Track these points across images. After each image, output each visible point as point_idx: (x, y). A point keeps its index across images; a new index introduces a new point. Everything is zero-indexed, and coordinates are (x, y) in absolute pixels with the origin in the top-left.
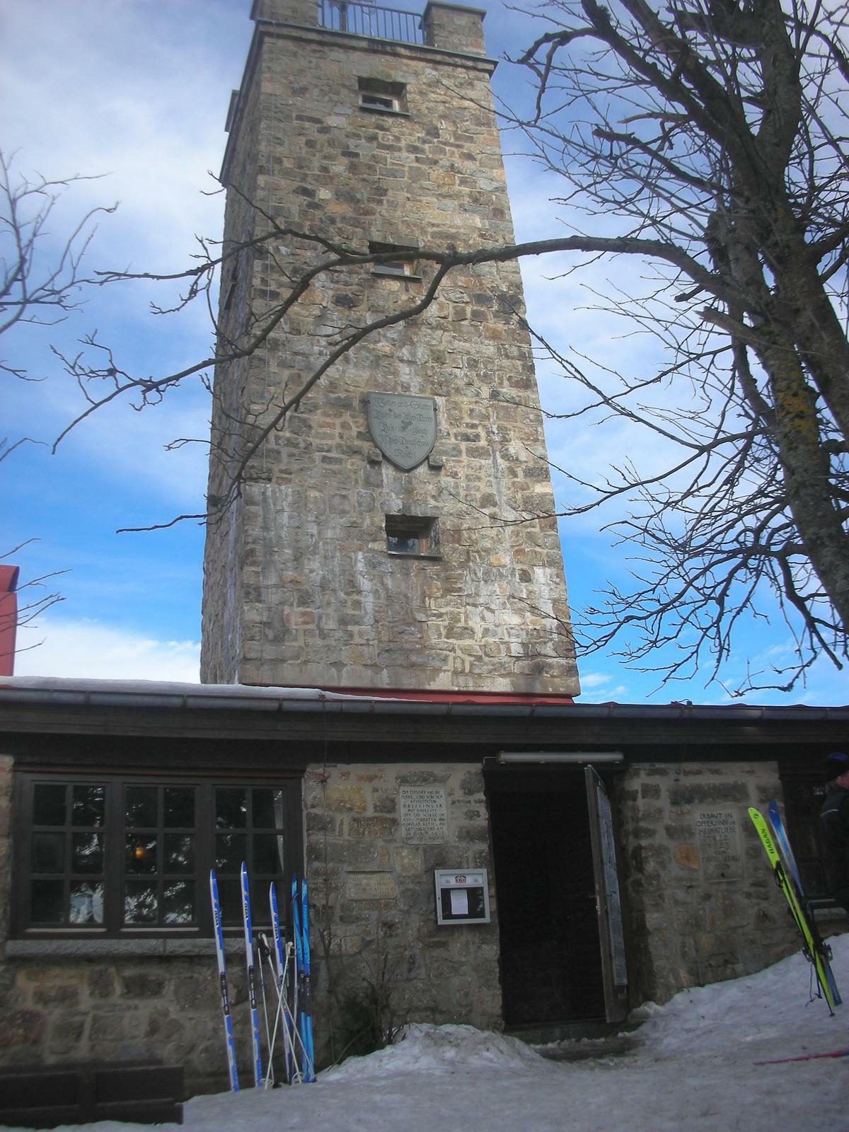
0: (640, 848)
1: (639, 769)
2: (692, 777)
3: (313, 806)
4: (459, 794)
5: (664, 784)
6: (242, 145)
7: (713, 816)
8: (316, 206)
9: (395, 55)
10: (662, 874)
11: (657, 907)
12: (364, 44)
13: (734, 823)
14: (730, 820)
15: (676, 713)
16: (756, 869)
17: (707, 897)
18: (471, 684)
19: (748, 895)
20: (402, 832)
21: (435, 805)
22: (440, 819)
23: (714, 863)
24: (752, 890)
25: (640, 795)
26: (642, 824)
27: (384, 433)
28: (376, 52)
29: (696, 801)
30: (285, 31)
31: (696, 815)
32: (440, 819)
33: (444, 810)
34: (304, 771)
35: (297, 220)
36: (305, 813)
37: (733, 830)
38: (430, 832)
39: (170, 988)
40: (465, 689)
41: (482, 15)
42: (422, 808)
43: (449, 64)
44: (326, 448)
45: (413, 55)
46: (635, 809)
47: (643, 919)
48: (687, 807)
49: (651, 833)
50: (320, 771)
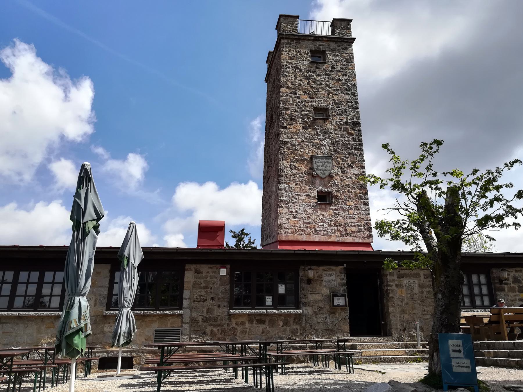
0: (388, 289)
2: (404, 271)
3: (302, 277)
4: (339, 274)
6: (273, 72)
8: (298, 98)
10: (394, 297)
11: (393, 306)
12: (312, 38)
14: (415, 283)
15: (399, 254)
16: (422, 297)
17: (407, 304)
19: (420, 304)
20: (324, 283)
23: (409, 295)
24: (420, 303)
25: (388, 275)
26: (388, 283)
29: (405, 277)
34: (300, 268)
36: (299, 278)
39: (267, 323)
46: (387, 279)
47: (388, 309)
49: (391, 286)
50: (303, 267)
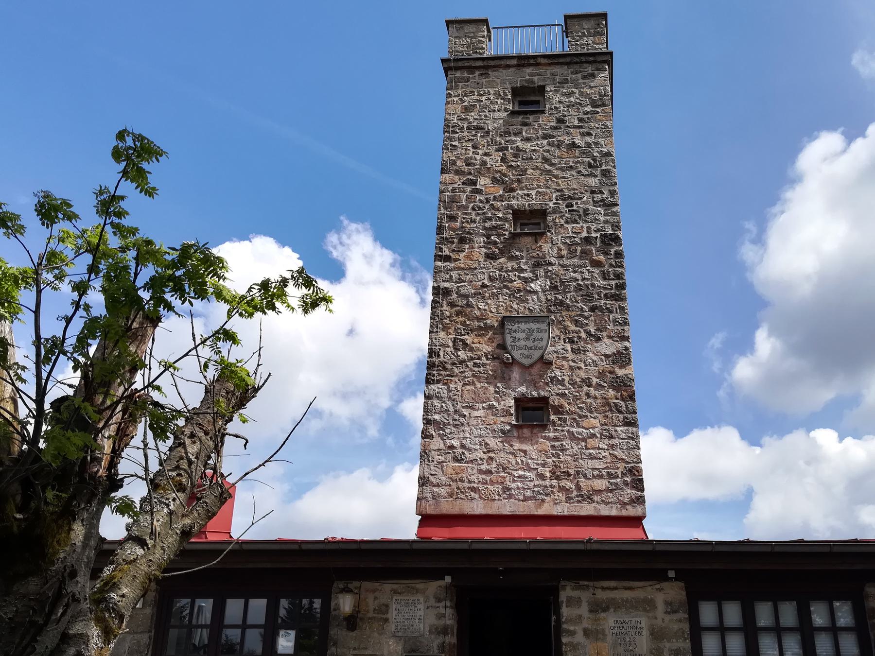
1: (566, 585)
4: (432, 602)
5: (585, 596)
7: (624, 622)
9: (537, 65)
12: (514, 62)
13: (642, 628)
14: (639, 626)
18: (566, 510)
20: (392, 627)
21: (416, 609)
22: (419, 619)
27: (513, 344)
28: (523, 66)
29: (612, 610)
30: (460, 64)
31: (610, 620)
32: (419, 619)
33: (421, 613)
35: (464, 203)
37: (641, 634)
38: (411, 628)
40: (562, 514)
41: (604, 16)
42: (407, 611)
43: (576, 63)
44: (476, 357)
45: (550, 61)
48: (603, 615)
49: (572, 633)
